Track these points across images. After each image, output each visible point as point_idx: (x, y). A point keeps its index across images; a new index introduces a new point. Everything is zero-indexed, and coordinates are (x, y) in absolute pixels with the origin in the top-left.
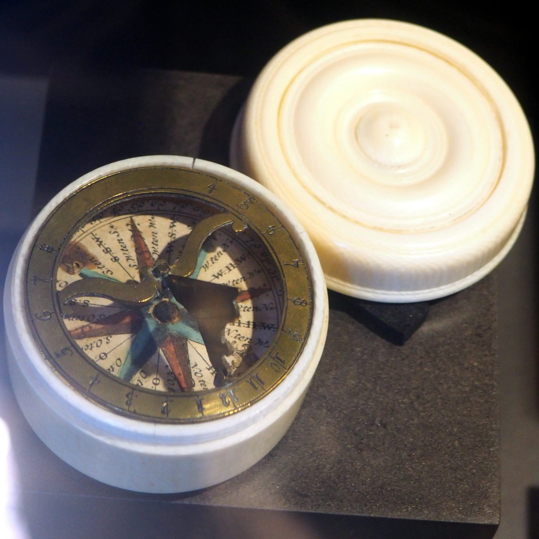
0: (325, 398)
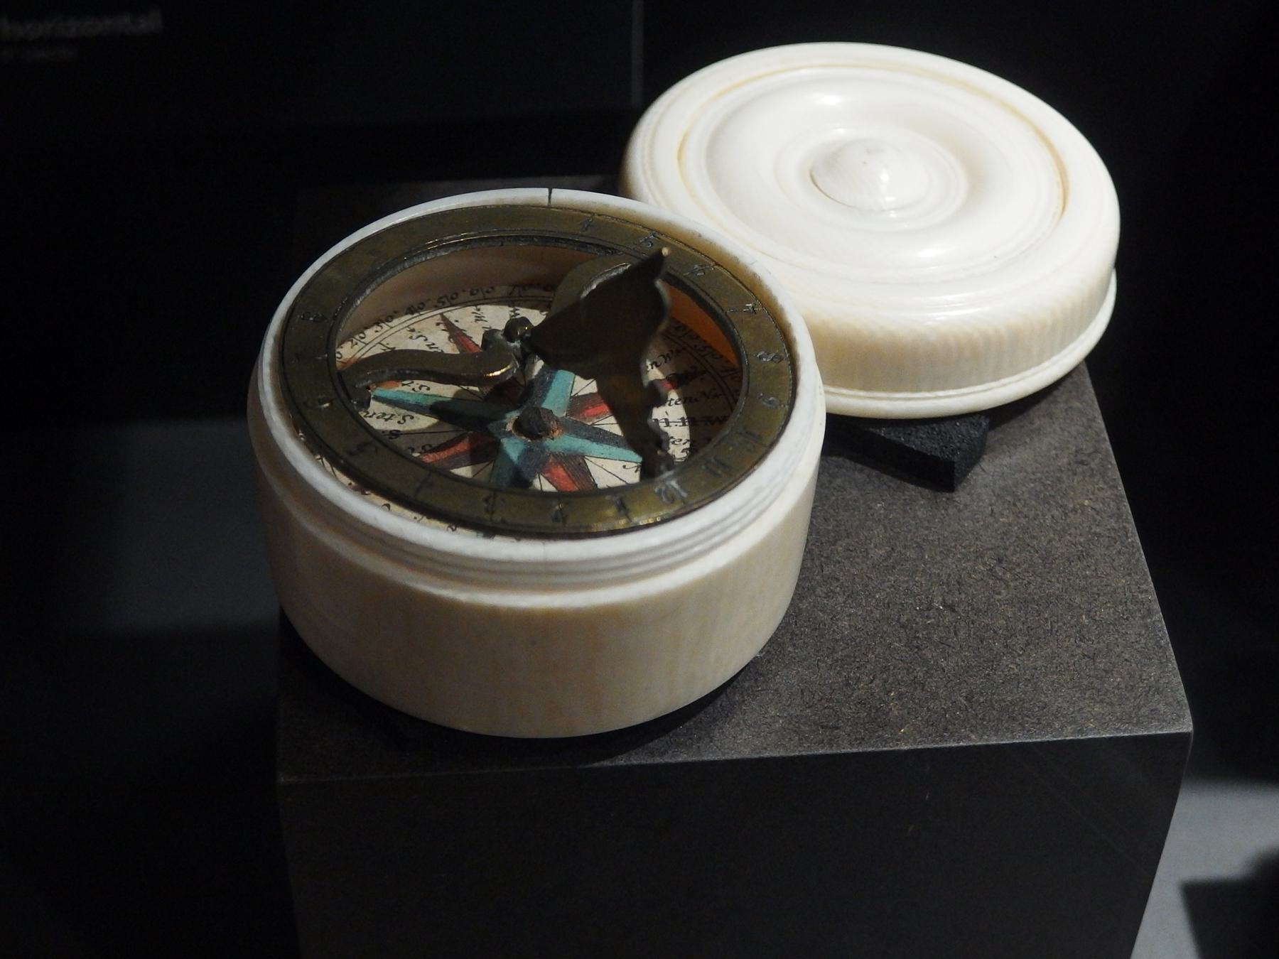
0: (838, 580)
